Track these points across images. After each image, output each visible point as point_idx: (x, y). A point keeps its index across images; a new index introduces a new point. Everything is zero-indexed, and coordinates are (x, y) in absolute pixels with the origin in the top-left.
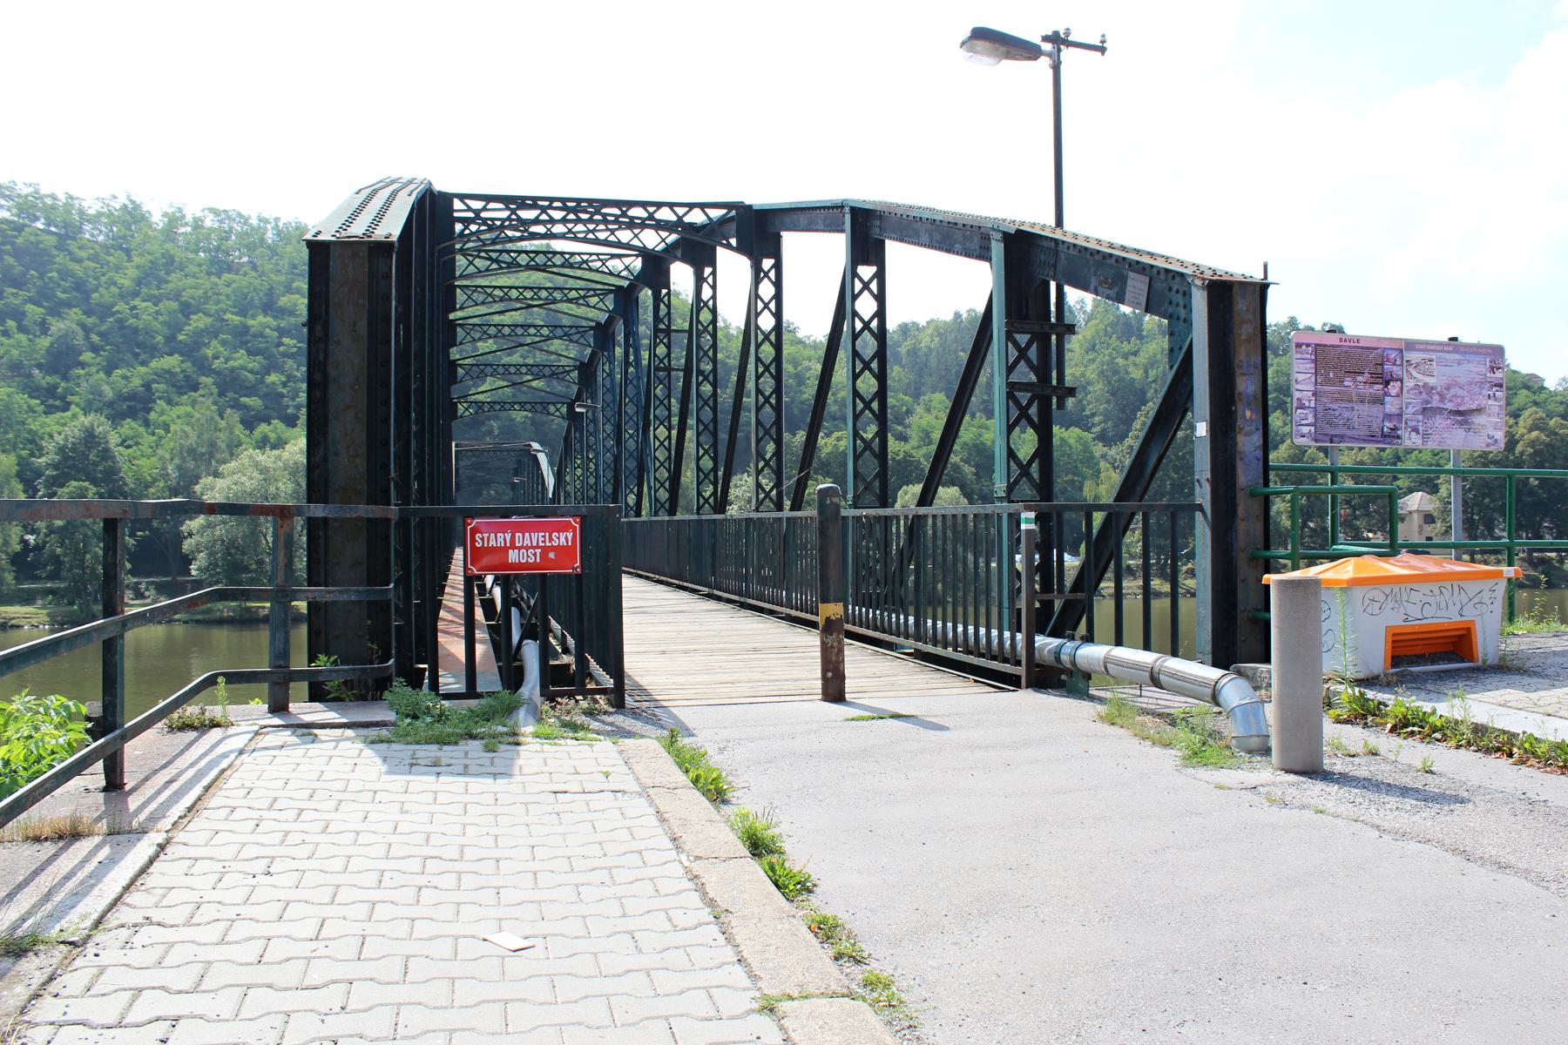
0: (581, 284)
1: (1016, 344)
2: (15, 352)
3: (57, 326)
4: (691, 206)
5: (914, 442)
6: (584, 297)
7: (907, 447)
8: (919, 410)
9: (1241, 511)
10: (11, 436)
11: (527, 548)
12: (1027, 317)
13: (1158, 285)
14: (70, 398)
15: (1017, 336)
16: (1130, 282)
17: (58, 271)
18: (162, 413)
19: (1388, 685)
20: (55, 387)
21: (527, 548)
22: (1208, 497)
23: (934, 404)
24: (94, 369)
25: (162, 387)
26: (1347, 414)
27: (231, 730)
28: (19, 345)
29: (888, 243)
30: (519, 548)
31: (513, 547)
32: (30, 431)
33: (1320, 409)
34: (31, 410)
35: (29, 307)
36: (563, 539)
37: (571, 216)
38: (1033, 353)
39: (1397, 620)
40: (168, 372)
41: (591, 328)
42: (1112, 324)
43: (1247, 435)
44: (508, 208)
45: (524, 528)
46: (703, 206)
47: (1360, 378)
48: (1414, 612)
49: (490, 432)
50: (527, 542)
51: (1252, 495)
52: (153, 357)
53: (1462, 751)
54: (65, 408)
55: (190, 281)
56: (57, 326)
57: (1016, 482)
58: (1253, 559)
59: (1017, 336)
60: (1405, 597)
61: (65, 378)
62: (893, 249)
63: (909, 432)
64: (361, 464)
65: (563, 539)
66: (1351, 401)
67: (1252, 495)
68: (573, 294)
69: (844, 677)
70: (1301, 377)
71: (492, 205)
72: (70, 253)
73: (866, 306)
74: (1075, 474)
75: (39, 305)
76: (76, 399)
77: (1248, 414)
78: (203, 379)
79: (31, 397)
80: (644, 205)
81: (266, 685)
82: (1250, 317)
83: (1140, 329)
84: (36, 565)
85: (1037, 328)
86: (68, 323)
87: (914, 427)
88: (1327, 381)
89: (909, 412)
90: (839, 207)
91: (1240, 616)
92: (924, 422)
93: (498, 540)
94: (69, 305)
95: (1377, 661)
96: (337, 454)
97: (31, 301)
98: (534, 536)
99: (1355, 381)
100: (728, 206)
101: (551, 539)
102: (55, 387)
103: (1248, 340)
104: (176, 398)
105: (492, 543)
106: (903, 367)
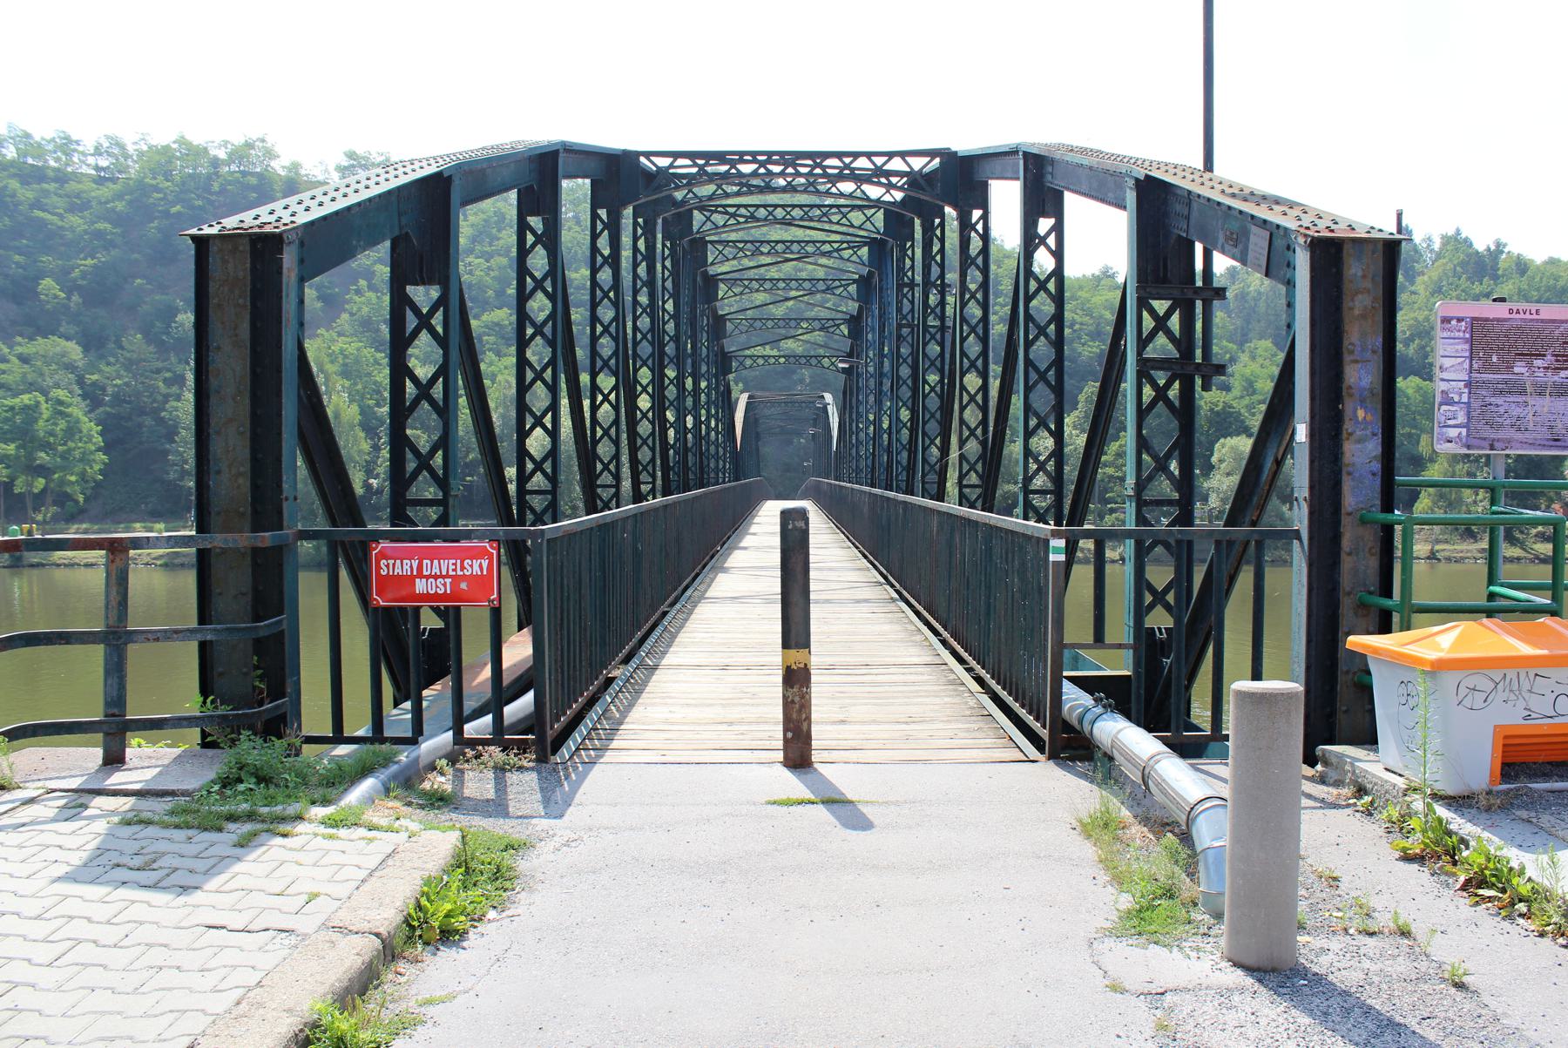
1: (1152, 312)
2: (365, 310)
4: (891, 155)
5: (1236, 392)
6: (838, 250)
7: (1230, 396)
8: (1244, 358)
9: (1346, 543)
10: (359, 387)
11: (436, 577)
12: (1165, 280)
13: (1279, 243)
15: (1156, 304)
16: (1252, 238)
18: (491, 364)
19: (1488, 809)
21: (436, 577)
22: (1306, 521)
23: (1259, 351)
25: (492, 339)
26: (1516, 411)
28: (369, 302)
29: (1067, 195)
30: (427, 577)
31: (420, 575)
32: (375, 383)
33: (1475, 405)
34: (377, 362)
36: (475, 567)
37: (790, 170)
38: (1175, 322)
39: (1512, 716)
40: (497, 324)
41: (855, 281)
42: (1463, 264)
43: (1359, 441)
44: (695, 165)
45: (434, 555)
46: (903, 155)
47: (1538, 363)
48: (1541, 706)
49: (802, 381)
50: (436, 571)
51: (1363, 522)
52: (484, 310)
53: (1547, 941)
57: (1150, 478)
58: (1362, 607)
59: (1156, 304)
60: (1526, 685)
62: (1071, 201)
63: (1232, 380)
64: (245, 484)
65: (475, 567)
66: (1523, 392)
67: (1363, 522)
68: (827, 247)
69: (809, 737)
70: (1447, 362)
71: (680, 162)
73: (1043, 261)
74: (1415, 427)
77: (1361, 414)
79: (377, 350)
80: (839, 155)
81: (100, 736)
82: (1369, 285)
83: (1495, 268)
85: (1176, 293)
87: (1237, 376)
88: (1488, 367)
89: (1233, 360)
90: (1013, 152)
91: (1341, 678)
92: (1247, 371)
93: (404, 567)
95: (1480, 771)
96: (219, 472)
99: (1530, 366)
100: (932, 154)
101: (463, 568)
103: (1363, 316)
104: (504, 349)
105: (398, 571)
106: (1229, 314)
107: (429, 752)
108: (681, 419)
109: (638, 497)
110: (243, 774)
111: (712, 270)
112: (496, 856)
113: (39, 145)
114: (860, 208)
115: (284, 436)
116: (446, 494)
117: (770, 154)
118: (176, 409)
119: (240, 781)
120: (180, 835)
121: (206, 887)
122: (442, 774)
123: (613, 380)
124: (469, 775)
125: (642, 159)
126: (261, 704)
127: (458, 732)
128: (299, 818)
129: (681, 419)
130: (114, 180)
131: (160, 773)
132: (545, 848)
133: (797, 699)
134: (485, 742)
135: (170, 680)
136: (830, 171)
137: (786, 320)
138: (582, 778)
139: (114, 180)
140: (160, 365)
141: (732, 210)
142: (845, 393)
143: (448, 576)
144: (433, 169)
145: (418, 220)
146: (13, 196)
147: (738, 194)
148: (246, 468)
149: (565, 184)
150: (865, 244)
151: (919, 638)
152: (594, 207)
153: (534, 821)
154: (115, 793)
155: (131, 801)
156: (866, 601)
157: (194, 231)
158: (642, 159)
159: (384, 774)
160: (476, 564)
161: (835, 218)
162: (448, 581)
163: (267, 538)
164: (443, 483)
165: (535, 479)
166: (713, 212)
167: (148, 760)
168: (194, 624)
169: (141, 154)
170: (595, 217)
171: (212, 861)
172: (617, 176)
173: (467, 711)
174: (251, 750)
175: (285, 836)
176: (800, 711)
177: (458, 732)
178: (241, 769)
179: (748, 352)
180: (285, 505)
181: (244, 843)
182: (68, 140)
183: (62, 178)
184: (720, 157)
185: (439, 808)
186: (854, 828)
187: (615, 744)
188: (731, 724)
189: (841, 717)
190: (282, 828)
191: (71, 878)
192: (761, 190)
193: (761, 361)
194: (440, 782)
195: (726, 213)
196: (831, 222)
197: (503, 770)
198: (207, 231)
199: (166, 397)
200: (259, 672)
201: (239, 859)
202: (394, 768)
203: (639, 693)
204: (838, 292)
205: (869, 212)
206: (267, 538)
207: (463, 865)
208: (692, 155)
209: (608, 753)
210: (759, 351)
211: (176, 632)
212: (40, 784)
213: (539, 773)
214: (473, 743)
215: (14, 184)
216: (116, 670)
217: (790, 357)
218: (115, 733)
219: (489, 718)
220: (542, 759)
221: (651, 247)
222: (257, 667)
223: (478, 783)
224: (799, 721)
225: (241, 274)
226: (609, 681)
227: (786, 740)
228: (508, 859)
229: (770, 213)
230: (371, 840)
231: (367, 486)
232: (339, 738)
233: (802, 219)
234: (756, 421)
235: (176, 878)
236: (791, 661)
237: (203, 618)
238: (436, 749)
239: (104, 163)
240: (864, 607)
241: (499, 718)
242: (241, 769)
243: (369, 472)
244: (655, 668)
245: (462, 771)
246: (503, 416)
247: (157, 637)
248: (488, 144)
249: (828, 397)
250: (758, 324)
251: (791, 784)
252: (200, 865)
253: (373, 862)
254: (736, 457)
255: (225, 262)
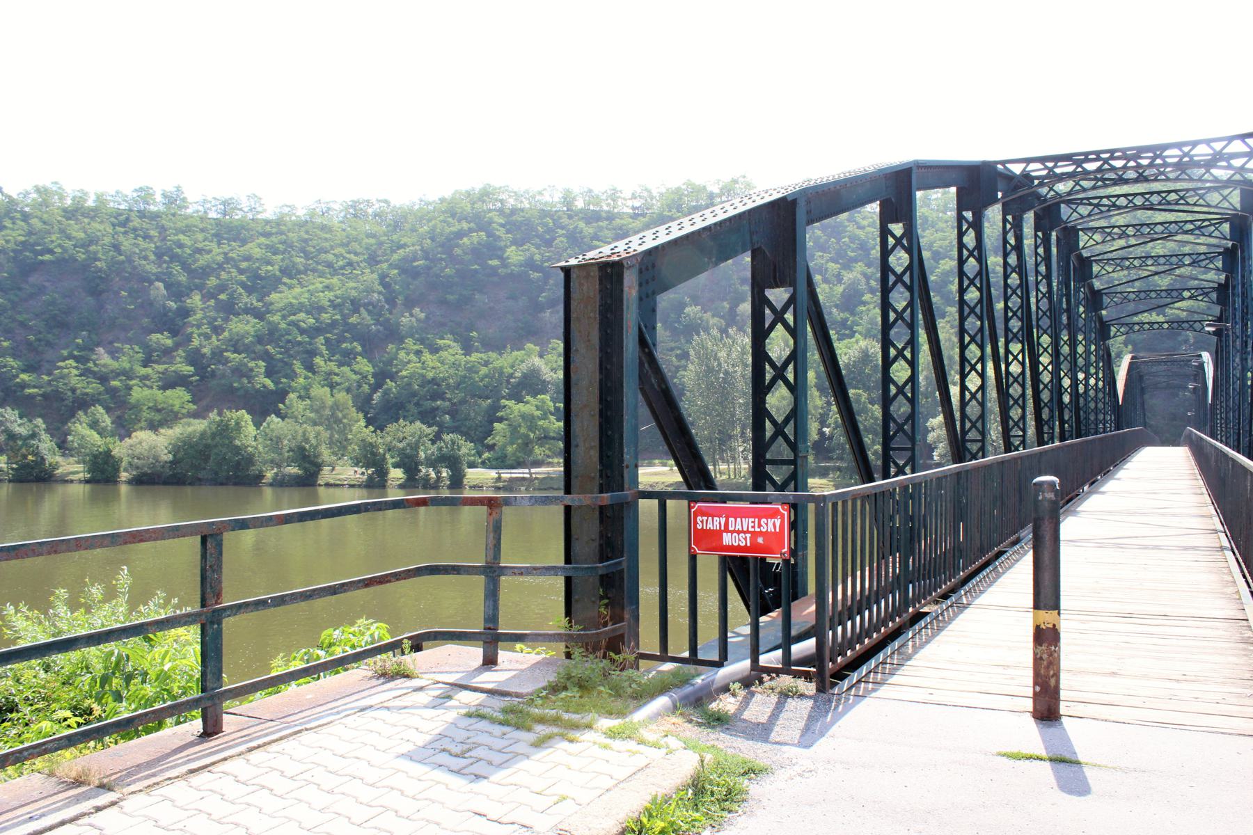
0: (1202, 217)
3: (848, 276)
4: (1230, 139)
6: (1199, 228)
11: (739, 532)
14: (856, 328)
17: (849, 237)
20: (846, 320)
21: (739, 532)
24: (872, 306)
27: (416, 683)
30: (732, 532)
35: (831, 265)
36: (770, 525)
41: (1220, 254)
45: (737, 514)
49: (1186, 341)
50: (739, 527)
54: (852, 336)
55: (939, 235)
56: (848, 276)
61: (853, 314)
64: (595, 454)
65: (770, 525)
72: (857, 223)
75: (836, 262)
76: (859, 328)
78: (949, 309)
84: (829, 450)
86: (855, 274)
93: (714, 523)
94: (855, 260)
96: (577, 446)
97: (832, 260)
98: (745, 521)
101: (760, 526)
102: (846, 320)
105: (710, 526)
107: (725, 677)
108: (1087, 379)
109: (1062, 439)
110: (568, 684)
111: (1085, 254)
112: (731, 780)
113: (598, 197)
114: (1216, 189)
115: (625, 417)
116: (796, 456)
117: (1112, 152)
118: (684, 376)
119: (565, 688)
120: (498, 730)
121: (492, 778)
122: (734, 695)
123: (1019, 346)
124: (758, 697)
125: (999, 166)
126: (605, 625)
127: (755, 660)
128: (589, 727)
129: (1087, 379)
130: (644, 215)
131: (514, 677)
132: (781, 775)
133: (1045, 656)
134: (778, 672)
135: (539, 600)
136: (1169, 160)
137: (1169, 291)
138: (848, 709)
139: (644, 215)
140: (673, 345)
141: (1095, 201)
142: (1217, 352)
143: (748, 532)
144: (780, 195)
145: (774, 236)
146: (581, 232)
147: (1094, 188)
148: (596, 443)
149: (919, 194)
150: (1226, 220)
151: (1231, 590)
152: (960, 209)
153: (785, 748)
154: (475, 690)
155: (484, 696)
156: (1195, 548)
157: (563, 264)
158: (999, 166)
159: (676, 694)
160: (770, 522)
161: (1191, 201)
162: (748, 535)
163: (606, 498)
164: (793, 446)
165: (897, 439)
166: (1078, 204)
167: (515, 662)
168: (561, 563)
169: (661, 194)
170: (960, 218)
171: (510, 755)
172: (977, 184)
173: (794, 633)
174: (589, 666)
175: (571, 741)
176: (1048, 668)
177: (755, 660)
178: (568, 679)
179: (1136, 319)
180: (626, 471)
181: (539, 744)
182: (615, 191)
183: (610, 217)
184: (1067, 158)
185: (713, 727)
186: (1071, 792)
187: (893, 680)
188: (1006, 667)
189: (1114, 669)
190: (572, 735)
191: (409, 757)
192: (1116, 182)
193: (1146, 326)
194: (727, 704)
195: (1090, 204)
196: (1188, 204)
197: (787, 696)
198: (573, 262)
199: (677, 368)
200: (606, 601)
201: (528, 757)
202: (688, 689)
203: (940, 629)
204: (1203, 263)
205: (1226, 192)
206: (606, 498)
207: (698, 788)
208: (1042, 160)
209: (885, 687)
210: (1145, 317)
211: (535, 568)
212: (432, 676)
213: (816, 701)
214: (769, 670)
215: (582, 224)
216: (492, 594)
217: (1177, 324)
218: (492, 641)
219: (779, 653)
220: (821, 689)
221: (1019, 238)
222: (602, 598)
223: (760, 707)
224: (1048, 677)
225: (592, 294)
226: (921, 616)
227: (1035, 693)
228: (744, 782)
229: (1131, 201)
230: (634, 753)
231: (821, 433)
232: (664, 657)
233: (1160, 204)
234: (1141, 378)
235: (476, 769)
236: (1040, 622)
237: (568, 560)
238: (731, 674)
239: (637, 203)
240: (1190, 555)
241: (787, 653)
242: (568, 679)
243: (823, 423)
244: (965, 607)
245: (753, 694)
246: (926, 378)
247: (522, 572)
248: (846, 169)
249: (1206, 357)
250: (1143, 295)
251: (1030, 735)
252: (497, 758)
253: (622, 774)
254: (1116, 409)
255: (581, 285)
